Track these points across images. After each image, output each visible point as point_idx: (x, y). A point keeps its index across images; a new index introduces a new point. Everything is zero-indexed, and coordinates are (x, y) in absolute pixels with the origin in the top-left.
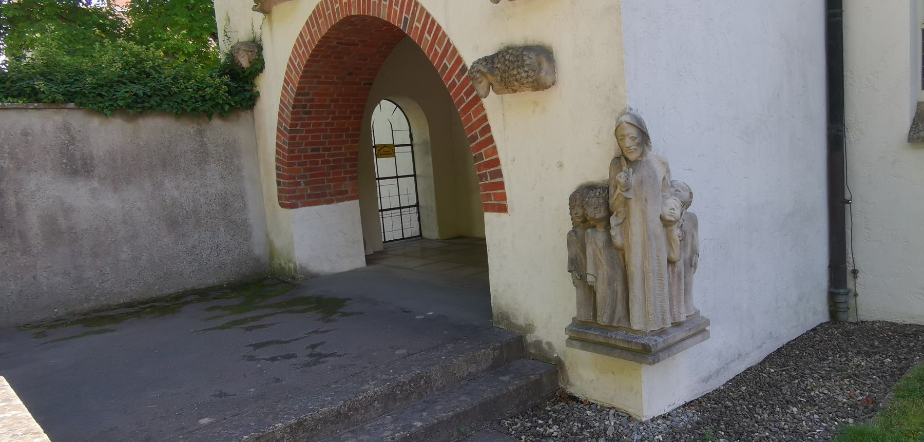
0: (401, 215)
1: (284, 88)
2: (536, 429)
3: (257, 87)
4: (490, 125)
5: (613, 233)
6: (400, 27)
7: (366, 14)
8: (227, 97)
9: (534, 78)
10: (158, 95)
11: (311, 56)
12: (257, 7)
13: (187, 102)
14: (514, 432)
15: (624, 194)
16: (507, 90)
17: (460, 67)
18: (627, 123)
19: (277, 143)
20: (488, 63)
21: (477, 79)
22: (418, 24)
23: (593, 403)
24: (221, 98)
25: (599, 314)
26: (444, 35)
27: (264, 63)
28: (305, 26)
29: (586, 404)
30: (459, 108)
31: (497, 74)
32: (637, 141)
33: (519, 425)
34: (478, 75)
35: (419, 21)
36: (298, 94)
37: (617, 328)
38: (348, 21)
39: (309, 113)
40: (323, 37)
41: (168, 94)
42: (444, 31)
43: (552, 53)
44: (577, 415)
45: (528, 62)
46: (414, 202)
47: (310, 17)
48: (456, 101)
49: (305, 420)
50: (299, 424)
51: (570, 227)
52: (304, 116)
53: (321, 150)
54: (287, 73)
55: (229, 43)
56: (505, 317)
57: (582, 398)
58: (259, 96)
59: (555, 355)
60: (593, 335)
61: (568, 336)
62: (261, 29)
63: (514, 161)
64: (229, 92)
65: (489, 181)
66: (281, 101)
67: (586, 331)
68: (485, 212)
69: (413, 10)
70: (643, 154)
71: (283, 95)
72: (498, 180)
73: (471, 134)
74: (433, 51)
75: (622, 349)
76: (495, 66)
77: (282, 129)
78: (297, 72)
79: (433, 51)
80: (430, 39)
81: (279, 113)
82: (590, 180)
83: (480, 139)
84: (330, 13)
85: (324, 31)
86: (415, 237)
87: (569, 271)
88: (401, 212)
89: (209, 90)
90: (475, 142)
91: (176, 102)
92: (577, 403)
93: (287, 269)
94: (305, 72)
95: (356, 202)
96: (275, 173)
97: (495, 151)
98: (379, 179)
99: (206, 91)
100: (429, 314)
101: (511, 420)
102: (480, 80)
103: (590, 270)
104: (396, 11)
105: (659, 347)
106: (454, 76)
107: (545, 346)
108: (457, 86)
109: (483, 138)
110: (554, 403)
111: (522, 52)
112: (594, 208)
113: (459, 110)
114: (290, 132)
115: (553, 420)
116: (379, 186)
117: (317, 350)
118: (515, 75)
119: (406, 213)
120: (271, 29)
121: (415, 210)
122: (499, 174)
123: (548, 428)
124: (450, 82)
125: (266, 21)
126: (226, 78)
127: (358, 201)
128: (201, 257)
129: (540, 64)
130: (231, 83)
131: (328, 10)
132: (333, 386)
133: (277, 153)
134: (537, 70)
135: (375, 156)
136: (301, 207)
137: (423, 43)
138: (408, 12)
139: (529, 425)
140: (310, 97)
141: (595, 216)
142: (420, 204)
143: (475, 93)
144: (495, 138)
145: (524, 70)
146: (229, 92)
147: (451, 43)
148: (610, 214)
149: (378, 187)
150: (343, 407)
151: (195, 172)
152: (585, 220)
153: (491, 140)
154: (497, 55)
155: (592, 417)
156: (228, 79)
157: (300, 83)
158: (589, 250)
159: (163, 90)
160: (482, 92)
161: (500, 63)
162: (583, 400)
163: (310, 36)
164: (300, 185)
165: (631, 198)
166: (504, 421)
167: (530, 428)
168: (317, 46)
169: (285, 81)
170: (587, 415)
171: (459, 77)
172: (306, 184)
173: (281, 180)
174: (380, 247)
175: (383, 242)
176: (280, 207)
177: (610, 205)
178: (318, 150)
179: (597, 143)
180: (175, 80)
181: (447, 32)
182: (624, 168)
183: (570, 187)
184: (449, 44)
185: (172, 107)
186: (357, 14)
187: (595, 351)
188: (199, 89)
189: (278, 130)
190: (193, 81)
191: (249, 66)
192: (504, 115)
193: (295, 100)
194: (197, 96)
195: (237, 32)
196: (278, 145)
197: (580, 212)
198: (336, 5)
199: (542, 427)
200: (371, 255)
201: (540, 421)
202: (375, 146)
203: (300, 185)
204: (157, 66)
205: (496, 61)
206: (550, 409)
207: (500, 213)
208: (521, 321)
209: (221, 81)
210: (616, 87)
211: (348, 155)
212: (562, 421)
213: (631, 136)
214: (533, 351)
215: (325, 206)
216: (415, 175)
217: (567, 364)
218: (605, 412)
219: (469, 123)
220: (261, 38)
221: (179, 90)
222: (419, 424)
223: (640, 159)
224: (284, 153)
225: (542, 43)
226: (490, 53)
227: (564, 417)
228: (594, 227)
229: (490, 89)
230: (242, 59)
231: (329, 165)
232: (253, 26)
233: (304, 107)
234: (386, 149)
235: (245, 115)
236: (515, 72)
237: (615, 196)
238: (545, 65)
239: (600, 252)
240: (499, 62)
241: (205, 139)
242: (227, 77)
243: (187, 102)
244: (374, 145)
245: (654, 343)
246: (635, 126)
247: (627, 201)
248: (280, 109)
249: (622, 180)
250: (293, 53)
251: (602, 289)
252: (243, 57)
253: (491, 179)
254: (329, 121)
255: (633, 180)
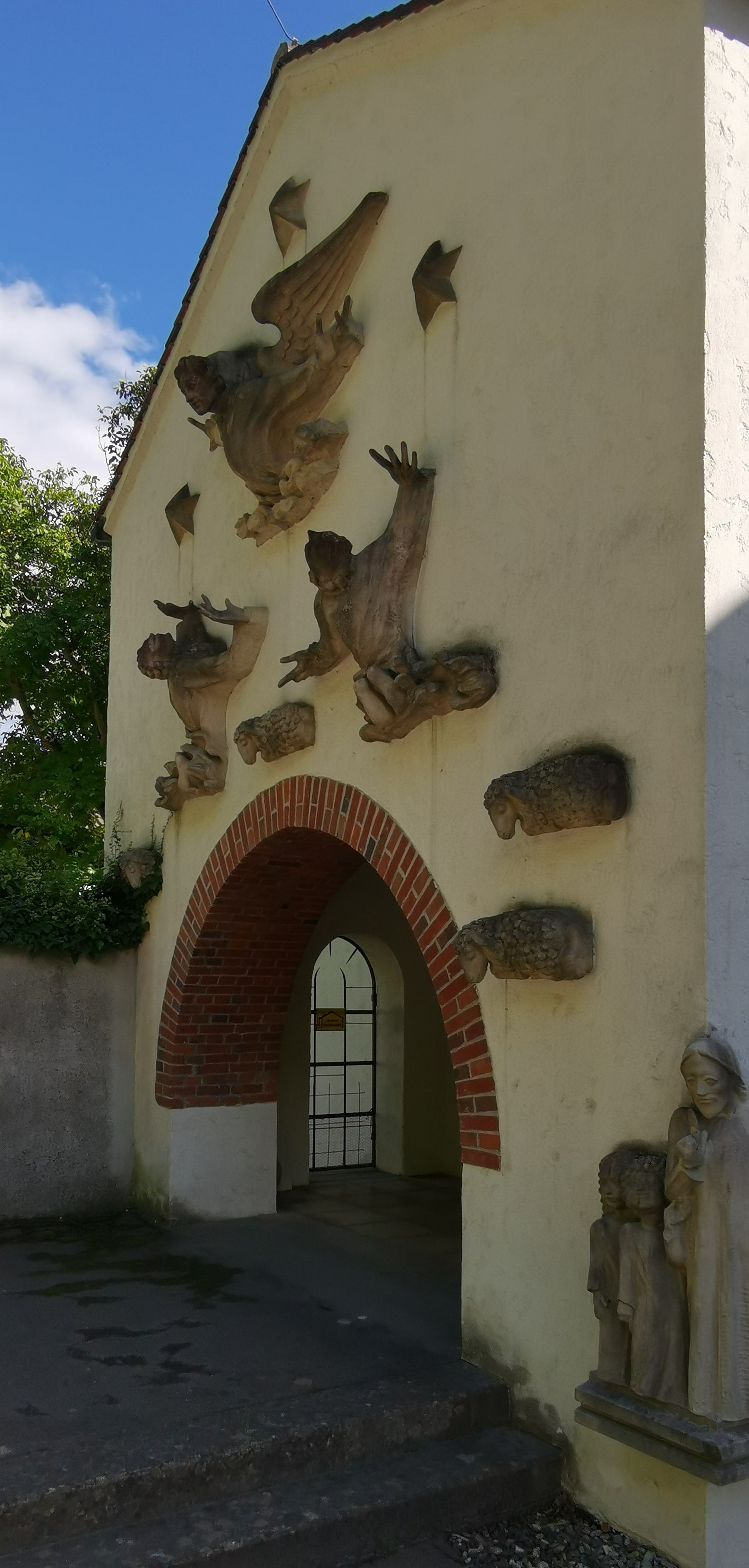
0: (345, 1127)
1: (185, 922)
2: (509, 1561)
3: (148, 917)
4: (484, 1023)
5: (667, 1236)
6: (362, 852)
7: (315, 828)
8: (102, 930)
9: (557, 961)
10: (12, 924)
11: (229, 879)
12: (162, 802)
13: (47, 934)
14: (469, 1559)
15: (690, 1174)
16: (513, 974)
17: (446, 926)
18: (702, 1055)
19: (164, 1003)
20: (486, 929)
21: (467, 953)
22: (389, 853)
23: (618, 1533)
24: (94, 930)
25: (634, 1374)
26: (427, 873)
27: (162, 882)
28: (226, 835)
29: (606, 1530)
30: (438, 989)
31: (500, 948)
32: (717, 1086)
33: (481, 1547)
34: (469, 948)
35: (390, 848)
36: (203, 934)
37: (664, 1405)
38: (289, 833)
39: (217, 962)
40: (250, 854)
41: (24, 922)
42: (426, 868)
43: (590, 922)
44: (585, 1549)
45: (548, 935)
46: (368, 1108)
47: (235, 823)
48: (434, 978)
49: (140, 1478)
50: (131, 1482)
51: (597, 1213)
52: (209, 967)
53: (228, 1020)
54: (191, 901)
55: (117, 847)
56: (482, 1347)
57: (600, 1518)
58: (161, 889)
59: (559, 1431)
60: (621, 1409)
61: (580, 1404)
62: (163, 831)
63: (517, 1086)
64: (107, 922)
65: (475, 1113)
66: (179, 942)
67: (611, 1401)
68: (465, 1162)
69: (383, 830)
70: (729, 1107)
71: (182, 932)
72: (489, 1114)
73: (454, 1033)
74: (408, 896)
75: (670, 1445)
76: (497, 936)
77: (175, 984)
78: (193, 936)
79: (408, 896)
80: (405, 877)
81: (173, 959)
82: (637, 1138)
83: (466, 1044)
84: (263, 820)
85: (252, 846)
86: (364, 1166)
87: (590, 1290)
88: (345, 1122)
89: (79, 919)
90: (458, 1047)
91: (34, 934)
92: (590, 1525)
93: (155, 1203)
94: (217, 902)
95: (273, 1105)
96: (157, 1050)
97: (488, 1065)
98: (315, 1065)
99: (75, 920)
100: (359, 1318)
101: (469, 1536)
102: (470, 955)
103: (624, 1295)
104: (358, 829)
105: (737, 1454)
106: (435, 938)
107: (544, 1412)
108: (438, 955)
109: (471, 1042)
110: (551, 1518)
111: (542, 918)
112: (638, 1190)
113: (438, 992)
114: (186, 989)
115: (541, 1550)
116: (315, 1076)
117: (178, 1357)
118: (526, 954)
119: (356, 1125)
120: (178, 833)
121: (367, 1120)
122: (492, 1104)
123: (530, 1563)
124: (428, 947)
125: (173, 821)
126: (105, 901)
127: (275, 1104)
128: (34, 1169)
129: (568, 940)
130: (112, 909)
131: (261, 815)
132: (190, 1426)
133: (163, 1018)
134: (562, 949)
135: (312, 1027)
136: (188, 1106)
137: (393, 881)
138: (375, 833)
139: (498, 1551)
140: (222, 938)
141: (639, 1203)
142: (378, 1111)
143: (462, 972)
144: (490, 1044)
145: (541, 948)
146: (107, 922)
147: (436, 887)
148: (665, 1202)
149: (312, 1079)
150: (199, 1465)
151: (43, 1039)
152: (622, 1206)
153: (483, 1047)
154: (502, 917)
155: (611, 1558)
156: (108, 902)
157: (208, 917)
158: (625, 1259)
159: (19, 917)
160: (472, 974)
161: (505, 931)
162: (601, 1523)
163: (231, 851)
164: (190, 1072)
165: (703, 1182)
166: (459, 1536)
167: (499, 1557)
168: (240, 866)
169: (188, 912)
170: (604, 1553)
171: (443, 940)
172: (200, 1071)
173: (164, 1062)
174: (303, 1179)
175: (311, 1170)
176: (156, 1103)
177: (665, 1188)
178: (224, 1019)
179: (654, 1078)
180: (37, 902)
181: (431, 870)
182: (693, 1129)
183: (604, 1146)
184: (432, 888)
185: (27, 942)
186: (301, 826)
187: (621, 1439)
188: (66, 916)
189: (169, 984)
190: (61, 904)
191: (140, 885)
192: (507, 1009)
193: (199, 943)
194: (62, 926)
195: (131, 831)
196: (165, 1007)
197: (615, 1191)
198: (272, 810)
199: (520, 1559)
200: (287, 1191)
201: (518, 1549)
202: (315, 1011)
203: (190, 1072)
204: (17, 880)
205: (500, 927)
206: (539, 1528)
207: (487, 1169)
208: (507, 1360)
209: (98, 905)
210: (690, 989)
211: (269, 1030)
212: (558, 1555)
213: (708, 1077)
214: (522, 1416)
215: (224, 1107)
216: (374, 1063)
217: (578, 1450)
218: (637, 1554)
219: (452, 1015)
220: (162, 844)
221: (39, 916)
222: (311, 1516)
223: (723, 1115)
224: (173, 1020)
225: (577, 904)
226: (493, 912)
227: (562, 1548)
228: (638, 1220)
229: (487, 969)
230: (132, 874)
231: (238, 1043)
232: (153, 827)
233: (211, 953)
234: (331, 1017)
235: (124, 957)
236: (527, 950)
237: (673, 1177)
238: (576, 943)
239: (644, 1268)
240: (504, 930)
241: (64, 990)
242: (107, 900)
243: (47, 934)
244: (312, 1009)
245: (727, 1446)
246: (716, 1061)
247: (693, 1186)
248: (175, 953)
249: (687, 1150)
250: (203, 872)
251: (641, 1331)
252: (133, 873)
253: (478, 1110)
254: (245, 975)
255: (708, 1150)
